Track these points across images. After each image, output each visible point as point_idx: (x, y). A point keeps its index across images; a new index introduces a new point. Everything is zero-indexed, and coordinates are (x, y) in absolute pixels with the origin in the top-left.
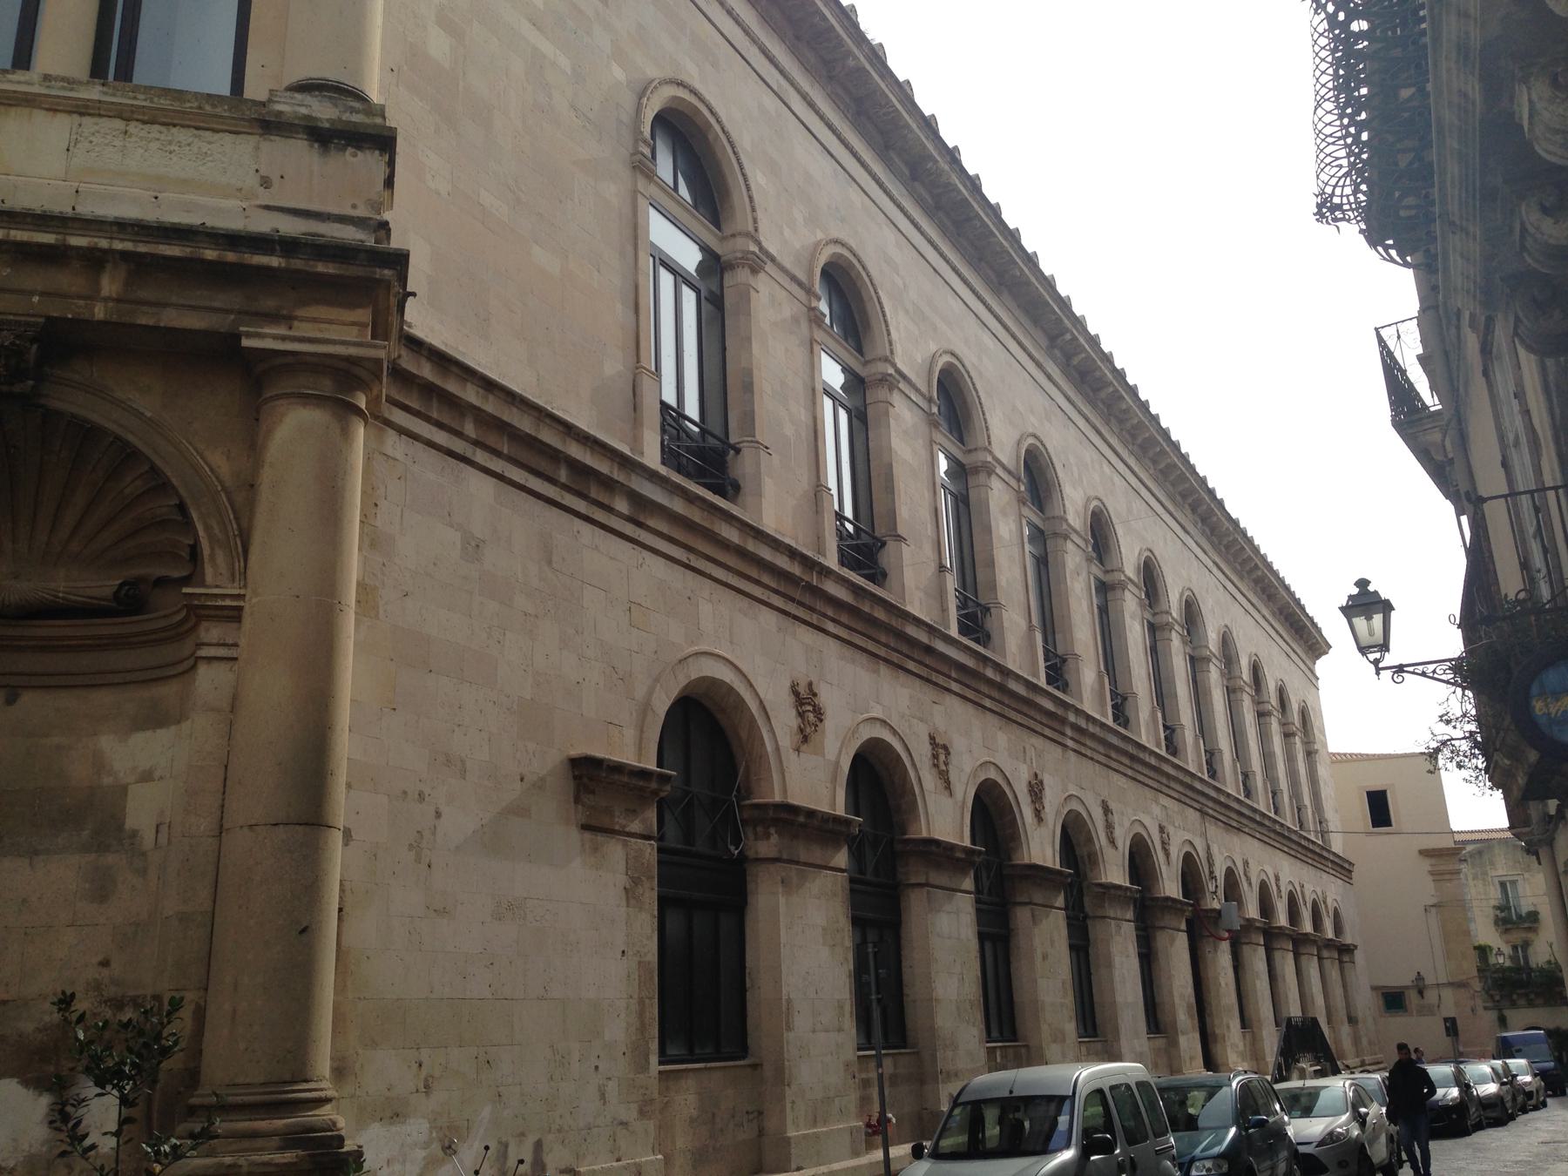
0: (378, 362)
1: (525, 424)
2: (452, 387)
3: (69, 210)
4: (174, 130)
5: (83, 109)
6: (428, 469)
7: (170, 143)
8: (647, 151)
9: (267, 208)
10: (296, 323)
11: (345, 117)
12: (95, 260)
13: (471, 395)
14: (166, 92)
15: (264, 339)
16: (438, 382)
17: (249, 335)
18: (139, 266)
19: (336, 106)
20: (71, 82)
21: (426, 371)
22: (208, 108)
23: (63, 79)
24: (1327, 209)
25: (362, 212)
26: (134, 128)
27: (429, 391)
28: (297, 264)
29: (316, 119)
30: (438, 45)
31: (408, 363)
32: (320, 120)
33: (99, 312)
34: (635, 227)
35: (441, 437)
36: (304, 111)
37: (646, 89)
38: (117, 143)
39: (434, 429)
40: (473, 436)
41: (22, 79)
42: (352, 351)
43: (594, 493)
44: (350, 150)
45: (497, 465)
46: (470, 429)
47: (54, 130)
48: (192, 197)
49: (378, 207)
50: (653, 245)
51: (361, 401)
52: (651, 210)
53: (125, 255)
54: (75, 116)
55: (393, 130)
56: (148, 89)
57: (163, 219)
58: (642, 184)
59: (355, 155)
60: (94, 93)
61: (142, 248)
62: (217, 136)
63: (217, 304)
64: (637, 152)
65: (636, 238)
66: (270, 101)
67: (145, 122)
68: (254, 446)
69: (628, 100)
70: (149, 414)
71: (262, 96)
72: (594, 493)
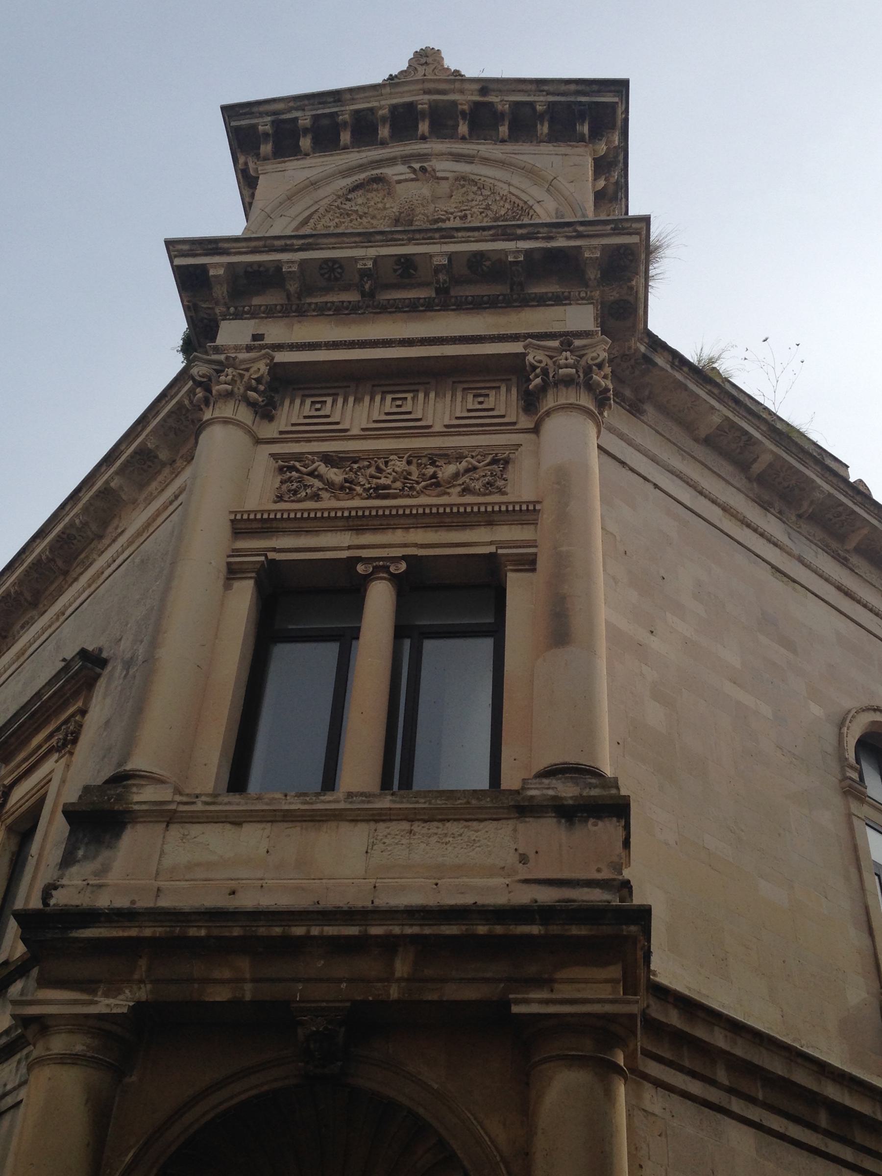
0: (632, 1017)
1: (777, 1066)
2: (700, 1032)
3: (369, 904)
4: (448, 824)
5: (379, 817)
6: (686, 1122)
7: (446, 835)
8: (855, 776)
9: (526, 881)
10: (556, 986)
11: (585, 793)
12: (389, 946)
13: (719, 1039)
14: (442, 793)
15: (531, 1004)
16: (687, 1029)
17: (518, 1002)
18: (425, 947)
19: (577, 784)
20: (367, 796)
21: (674, 1018)
22: (474, 802)
23: (362, 794)
24: (426, 58)
25: (606, 874)
26: (417, 827)
27: (679, 1038)
28: (555, 929)
29: (561, 798)
30: (655, 715)
31: (657, 1012)
32: (565, 798)
33: (394, 992)
34: (855, 848)
35: (695, 1087)
36: (551, 793)
37: (844, 720)
38: (404, 841)
39: (688, 1079)
40: (726, 1083)
41: (331, 798)
42: (608, 1008)
43: (860, 1137)
44: (591, 821)
45: (754, 1113)
46: (722, 1076)
47: (356, 837)
48: (466, 880)
49: (618, 868)
50: (876, 864)
51: (620, 1059)
52: (868, 829)
53: (415, 939)
54: (372, 824)
55: (627, 798)
56: (426, 794)
57: (443, 903)
58: (854, 807)
59: (596, 825)
60: (386, 803)
61: (427, 931)
62: (482, 825)
63: (489, 975)
64: (845, 778)
65: (857, 860)
66: (523, 788)
67: (425, 821)
68: (525, 1110)
69: (829, 733)
70: (436, 1086)
71: (516, 785)
72: (860, 1137)
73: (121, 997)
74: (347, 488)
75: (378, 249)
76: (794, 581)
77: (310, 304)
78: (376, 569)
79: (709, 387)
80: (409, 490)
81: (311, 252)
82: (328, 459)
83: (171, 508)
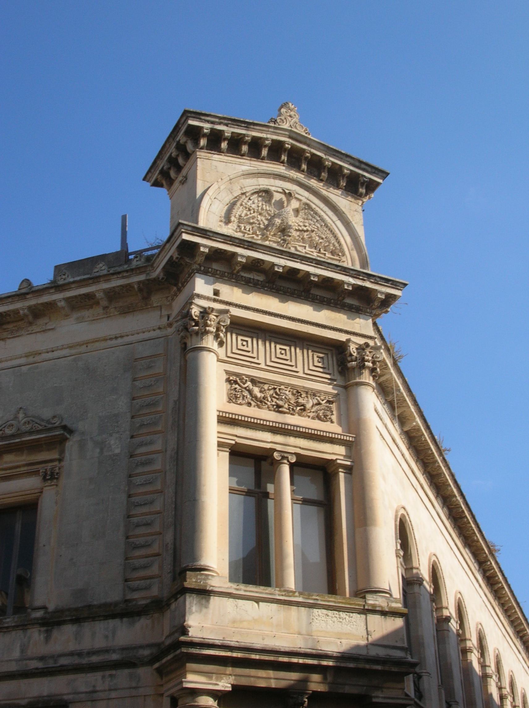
28: (387, 668)
73: (222, 681)
74: (260, 402)
75: (286, 261)
76: (384, 439)
77: (242, 276)
78: (283, 458)
79: (180, 126)
80: (292, 412)
81: (253, 252)
82: (254, 381)
83: (114, 342)
